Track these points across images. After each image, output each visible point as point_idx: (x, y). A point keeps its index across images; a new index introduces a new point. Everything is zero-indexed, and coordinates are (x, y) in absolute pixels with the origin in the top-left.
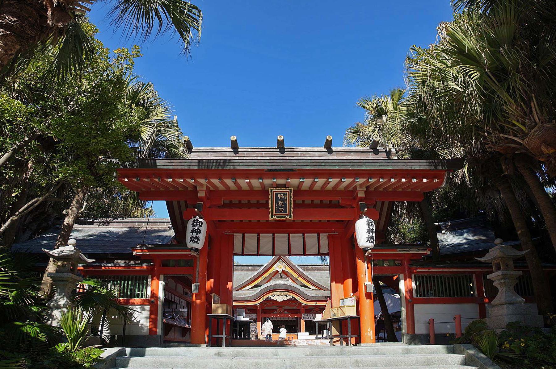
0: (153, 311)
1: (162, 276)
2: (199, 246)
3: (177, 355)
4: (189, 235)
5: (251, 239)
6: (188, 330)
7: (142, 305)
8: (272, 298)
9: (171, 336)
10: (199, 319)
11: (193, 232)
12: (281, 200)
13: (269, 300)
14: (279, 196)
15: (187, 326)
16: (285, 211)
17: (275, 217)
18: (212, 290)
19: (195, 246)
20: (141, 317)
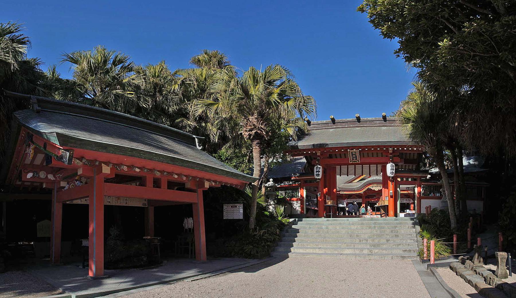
0: (302, 204)
1: (304, 188)
2: (320, 177)
3: (314, 221)
4: (315, 173)
5: (344, 168)
6: (317, 210)
7: (297, 200)
9: (309, 214)
10: (321, 206)
11: (317, 172)
13: (369, 190)
15: (316, 209)
18: (327, 193)
19: (318, 177)
20: (297, 206)
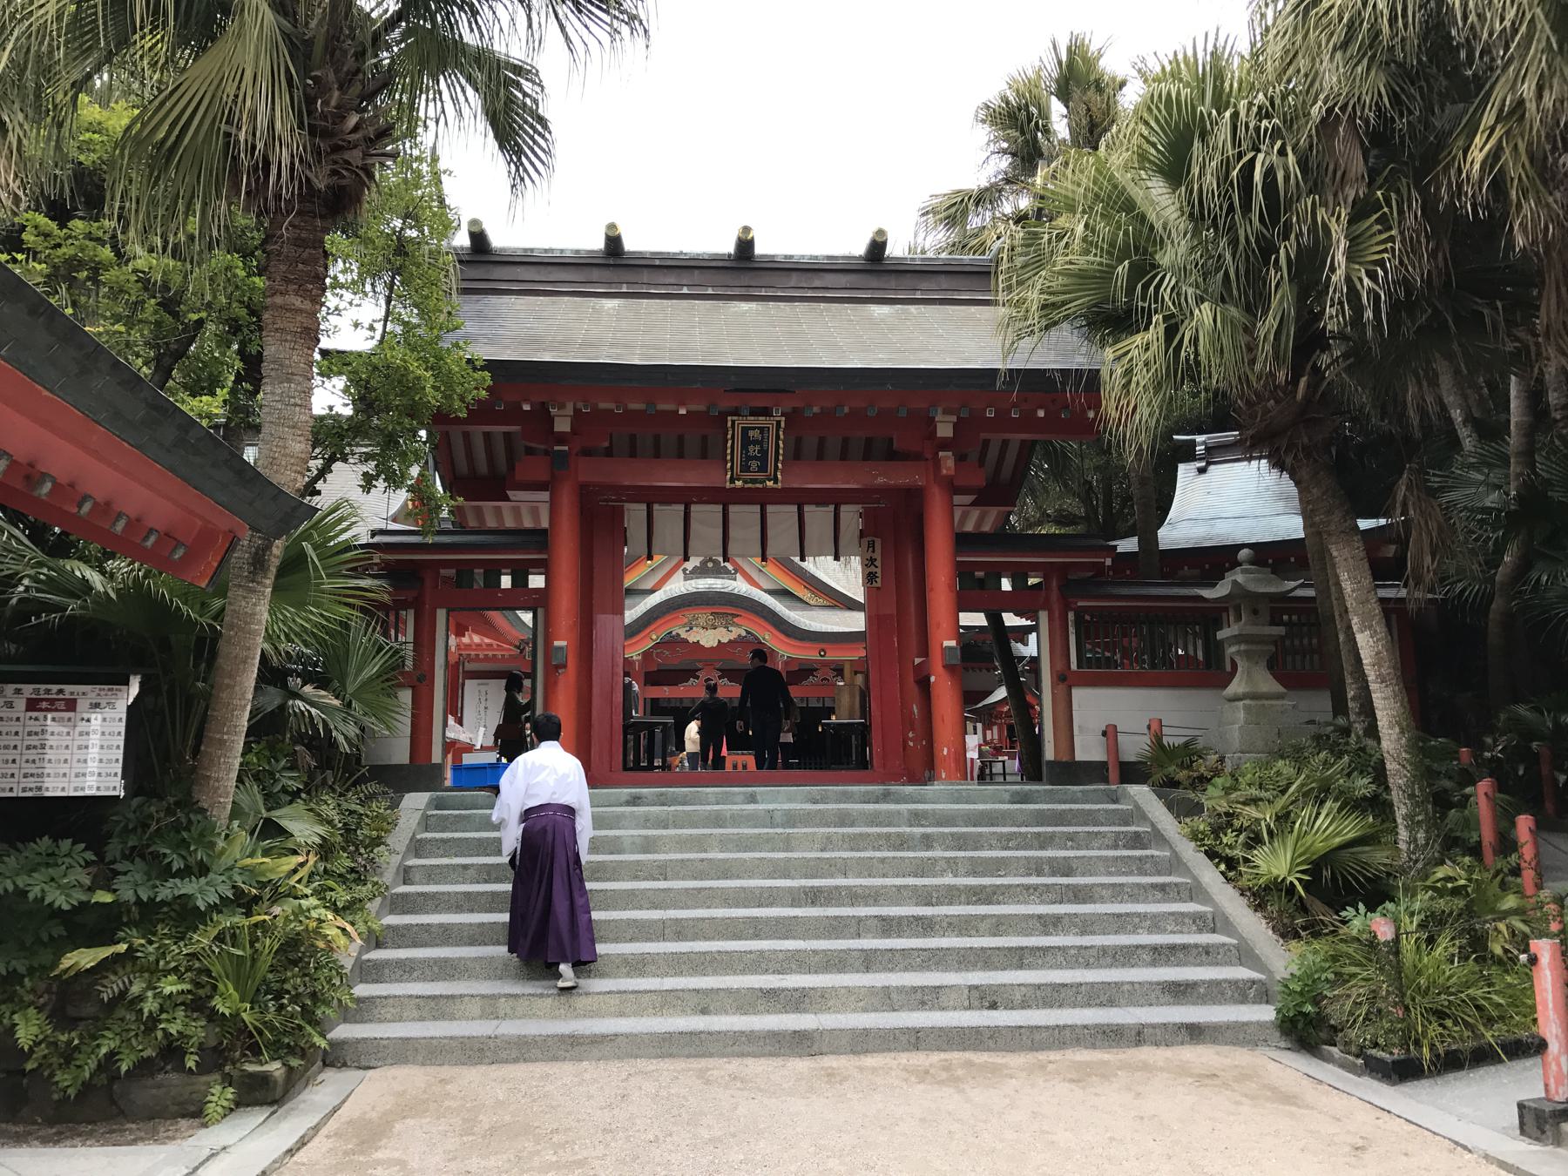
5: (669, 517)
8: (684, 635)
12: (755, 442)
13: (673, 642)
14: (751, 433)
16: (763, 468)
17: (739, 484)
